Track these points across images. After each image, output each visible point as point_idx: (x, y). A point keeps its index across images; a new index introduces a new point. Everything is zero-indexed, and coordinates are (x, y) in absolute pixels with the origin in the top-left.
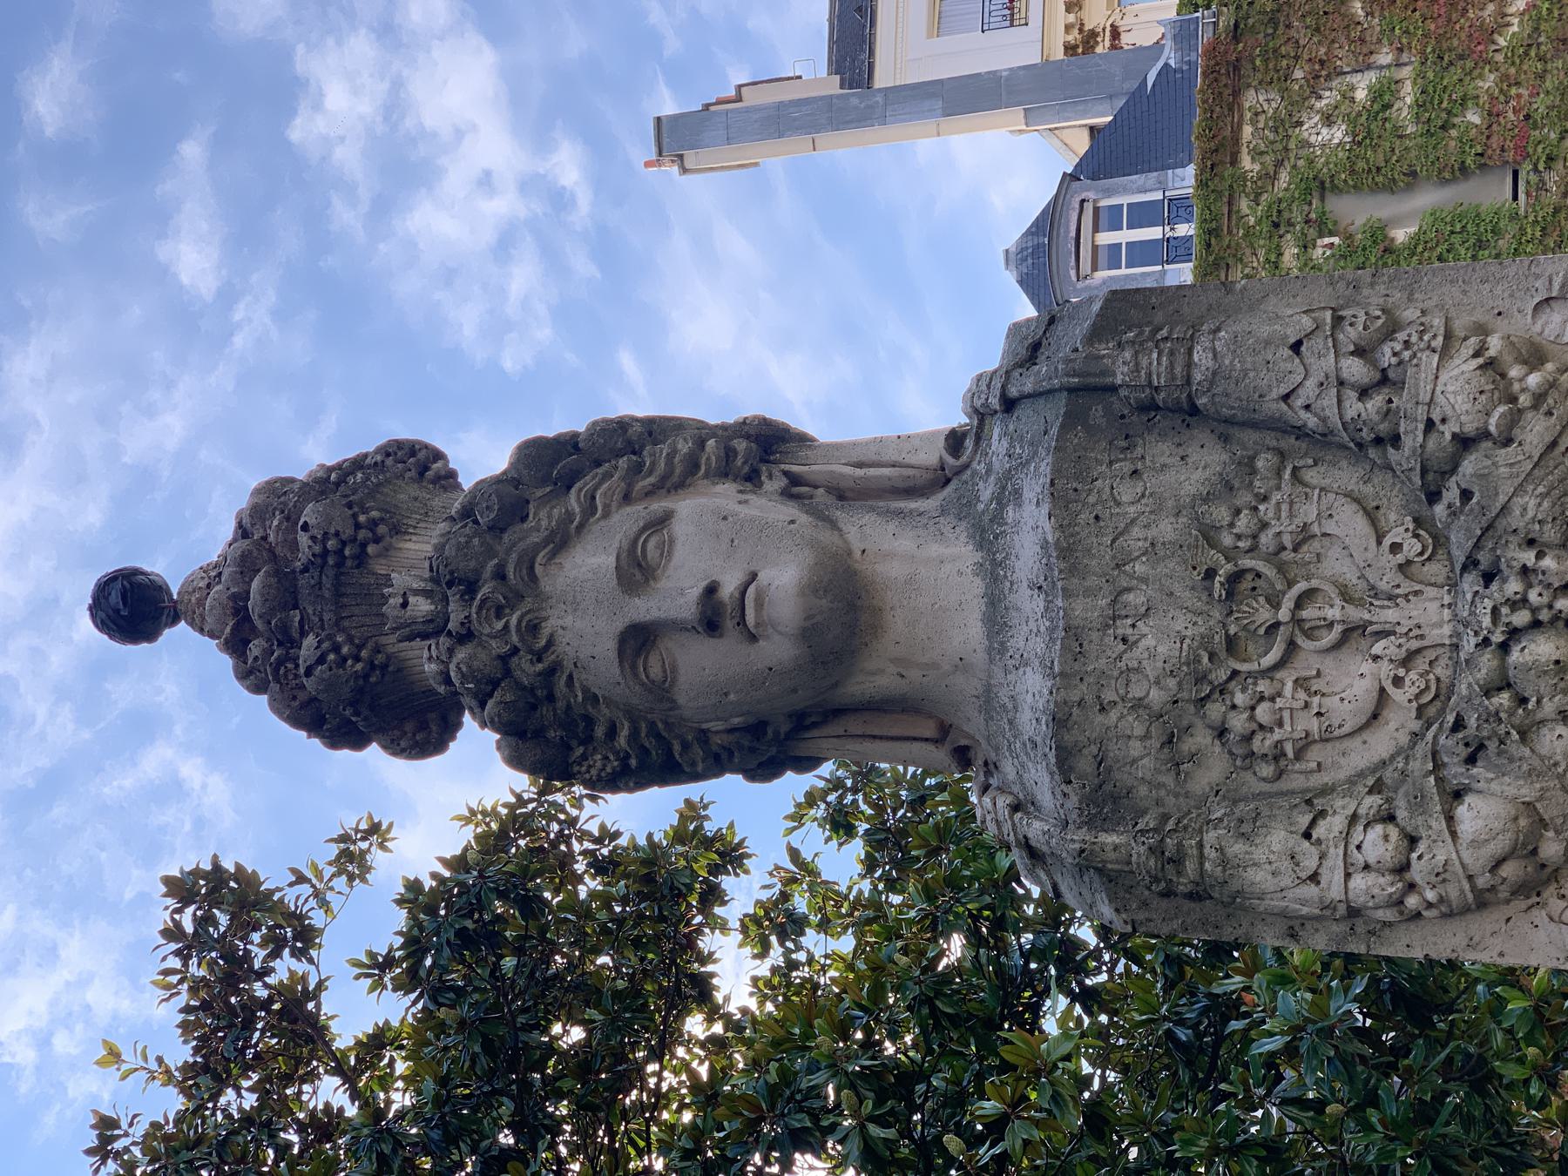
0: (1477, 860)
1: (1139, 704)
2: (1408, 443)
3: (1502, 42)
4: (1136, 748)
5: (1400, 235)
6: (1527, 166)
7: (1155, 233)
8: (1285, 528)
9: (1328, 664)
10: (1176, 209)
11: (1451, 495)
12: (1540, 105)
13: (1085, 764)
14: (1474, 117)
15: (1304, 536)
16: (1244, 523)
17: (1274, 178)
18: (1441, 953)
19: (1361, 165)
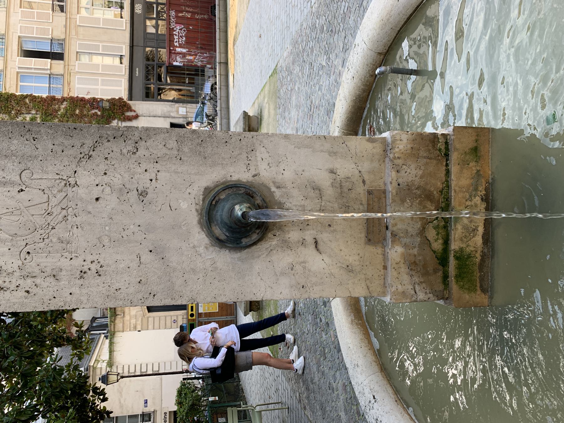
3: (59, 113)
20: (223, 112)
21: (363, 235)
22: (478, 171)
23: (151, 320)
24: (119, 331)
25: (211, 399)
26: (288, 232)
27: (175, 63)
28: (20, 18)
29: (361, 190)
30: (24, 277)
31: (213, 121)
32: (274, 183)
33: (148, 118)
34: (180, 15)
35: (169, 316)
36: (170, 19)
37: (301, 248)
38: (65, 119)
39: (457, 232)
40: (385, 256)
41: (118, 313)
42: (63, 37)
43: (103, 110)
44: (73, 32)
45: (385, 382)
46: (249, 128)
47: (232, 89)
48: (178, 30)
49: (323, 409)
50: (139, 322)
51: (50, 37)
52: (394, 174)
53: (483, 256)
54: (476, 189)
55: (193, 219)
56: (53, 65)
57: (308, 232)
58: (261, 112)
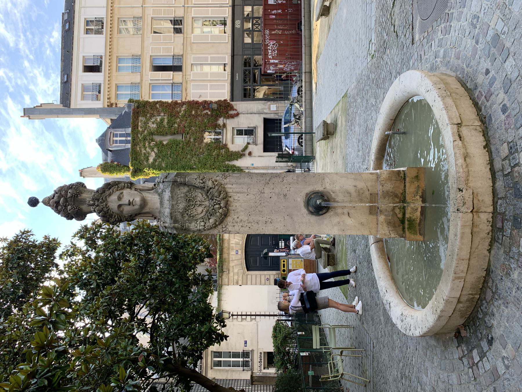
0: (211, 224)
1: (179, 212)
2: (206, 188)
3: (180, 114)
4: (179, 216)
5: (165, 143)
6: (184, 134)
7: (124, 139)
8: (194, 195)
9: (198, 208)
10: (127, 135)
11: (209, 193)
12: (186, 125)
13: (173, 218)
14: (176, 125)
15: (196, 196)
16: (190, 195)
17: (144, 132)
18: (207, 233)
19: (158, 131)
20: (307, 112)
21: (368, 211)
22: (418, 185)
23: (249, 277)
24: (225, 285)
25: (299, 333)
26: (337, 209)
27: (268, 71)
28: (151, 42)
29: (367, 193)
30: (249, 223)
31: (299, 120)
32: (332, 191)
33: (246, 115)
34: (273, 32)
35: (263, 275)
36: (265, 37)
37: (343, 216)
38: (185, 118)
39: (408, 211)
40: (377, 219)
41: (224, 270)
42: (181, 53)
43: (212, 110)
44: (189, 49)
45: (393, 284)
46: (327, 132)
47: (315, 94)
48: (271, 45)
49: (372, 319)
50: (240, 278)
51: (172, 54)
52: (381, 187)
53: (421, 220)
54: (417, 193)
55: (302, 204)
56: (174, 76)
57: (345, 210)
58: (336, 121)
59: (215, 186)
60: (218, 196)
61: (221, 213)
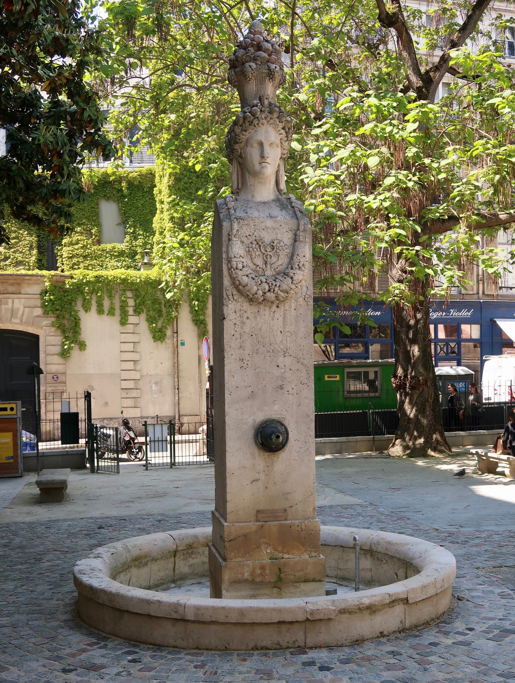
0: (239, 278)
59: (294, 284)
60: (281, 289)
61: (256, 294)
